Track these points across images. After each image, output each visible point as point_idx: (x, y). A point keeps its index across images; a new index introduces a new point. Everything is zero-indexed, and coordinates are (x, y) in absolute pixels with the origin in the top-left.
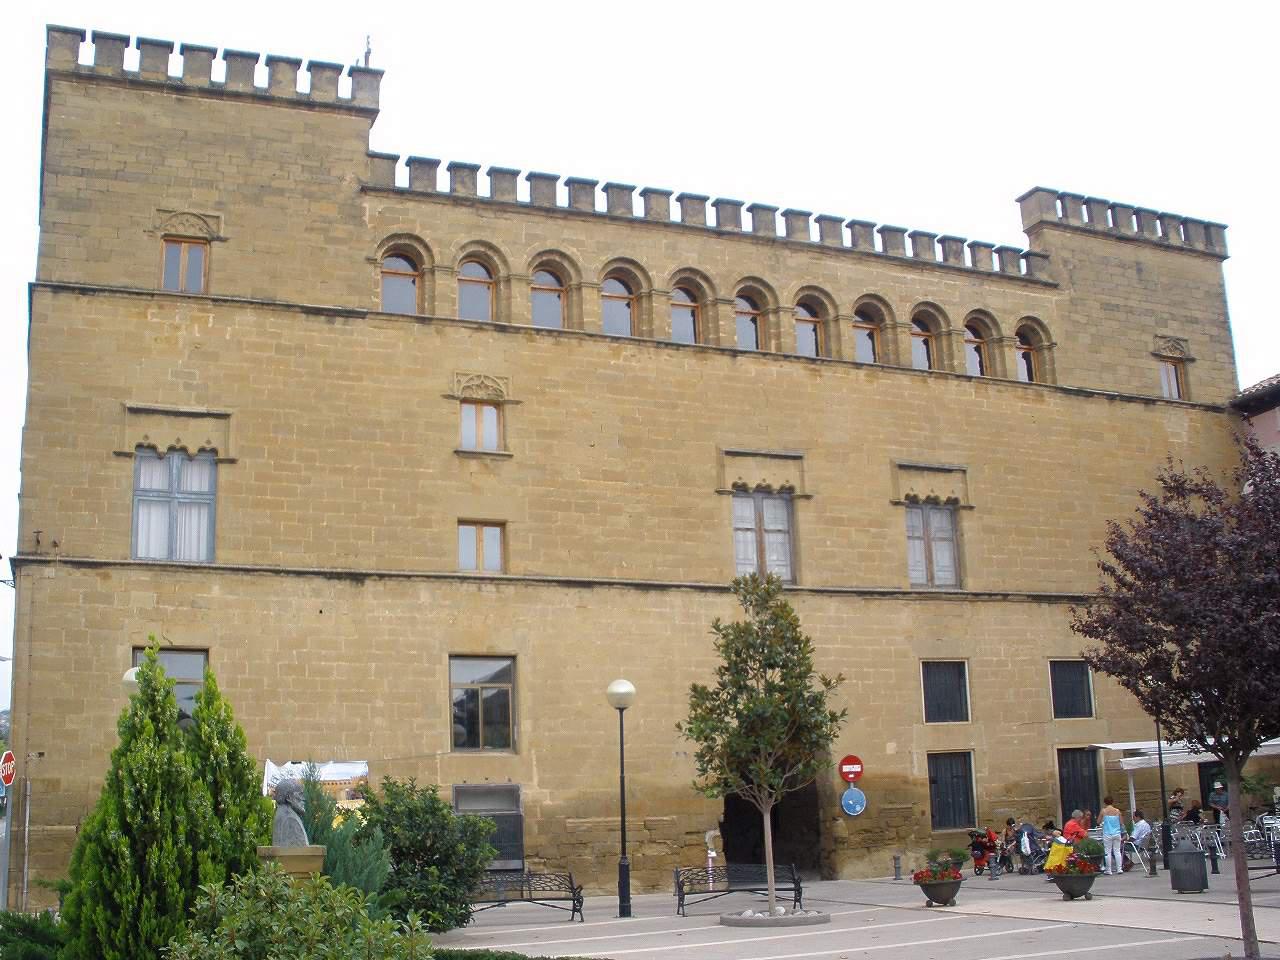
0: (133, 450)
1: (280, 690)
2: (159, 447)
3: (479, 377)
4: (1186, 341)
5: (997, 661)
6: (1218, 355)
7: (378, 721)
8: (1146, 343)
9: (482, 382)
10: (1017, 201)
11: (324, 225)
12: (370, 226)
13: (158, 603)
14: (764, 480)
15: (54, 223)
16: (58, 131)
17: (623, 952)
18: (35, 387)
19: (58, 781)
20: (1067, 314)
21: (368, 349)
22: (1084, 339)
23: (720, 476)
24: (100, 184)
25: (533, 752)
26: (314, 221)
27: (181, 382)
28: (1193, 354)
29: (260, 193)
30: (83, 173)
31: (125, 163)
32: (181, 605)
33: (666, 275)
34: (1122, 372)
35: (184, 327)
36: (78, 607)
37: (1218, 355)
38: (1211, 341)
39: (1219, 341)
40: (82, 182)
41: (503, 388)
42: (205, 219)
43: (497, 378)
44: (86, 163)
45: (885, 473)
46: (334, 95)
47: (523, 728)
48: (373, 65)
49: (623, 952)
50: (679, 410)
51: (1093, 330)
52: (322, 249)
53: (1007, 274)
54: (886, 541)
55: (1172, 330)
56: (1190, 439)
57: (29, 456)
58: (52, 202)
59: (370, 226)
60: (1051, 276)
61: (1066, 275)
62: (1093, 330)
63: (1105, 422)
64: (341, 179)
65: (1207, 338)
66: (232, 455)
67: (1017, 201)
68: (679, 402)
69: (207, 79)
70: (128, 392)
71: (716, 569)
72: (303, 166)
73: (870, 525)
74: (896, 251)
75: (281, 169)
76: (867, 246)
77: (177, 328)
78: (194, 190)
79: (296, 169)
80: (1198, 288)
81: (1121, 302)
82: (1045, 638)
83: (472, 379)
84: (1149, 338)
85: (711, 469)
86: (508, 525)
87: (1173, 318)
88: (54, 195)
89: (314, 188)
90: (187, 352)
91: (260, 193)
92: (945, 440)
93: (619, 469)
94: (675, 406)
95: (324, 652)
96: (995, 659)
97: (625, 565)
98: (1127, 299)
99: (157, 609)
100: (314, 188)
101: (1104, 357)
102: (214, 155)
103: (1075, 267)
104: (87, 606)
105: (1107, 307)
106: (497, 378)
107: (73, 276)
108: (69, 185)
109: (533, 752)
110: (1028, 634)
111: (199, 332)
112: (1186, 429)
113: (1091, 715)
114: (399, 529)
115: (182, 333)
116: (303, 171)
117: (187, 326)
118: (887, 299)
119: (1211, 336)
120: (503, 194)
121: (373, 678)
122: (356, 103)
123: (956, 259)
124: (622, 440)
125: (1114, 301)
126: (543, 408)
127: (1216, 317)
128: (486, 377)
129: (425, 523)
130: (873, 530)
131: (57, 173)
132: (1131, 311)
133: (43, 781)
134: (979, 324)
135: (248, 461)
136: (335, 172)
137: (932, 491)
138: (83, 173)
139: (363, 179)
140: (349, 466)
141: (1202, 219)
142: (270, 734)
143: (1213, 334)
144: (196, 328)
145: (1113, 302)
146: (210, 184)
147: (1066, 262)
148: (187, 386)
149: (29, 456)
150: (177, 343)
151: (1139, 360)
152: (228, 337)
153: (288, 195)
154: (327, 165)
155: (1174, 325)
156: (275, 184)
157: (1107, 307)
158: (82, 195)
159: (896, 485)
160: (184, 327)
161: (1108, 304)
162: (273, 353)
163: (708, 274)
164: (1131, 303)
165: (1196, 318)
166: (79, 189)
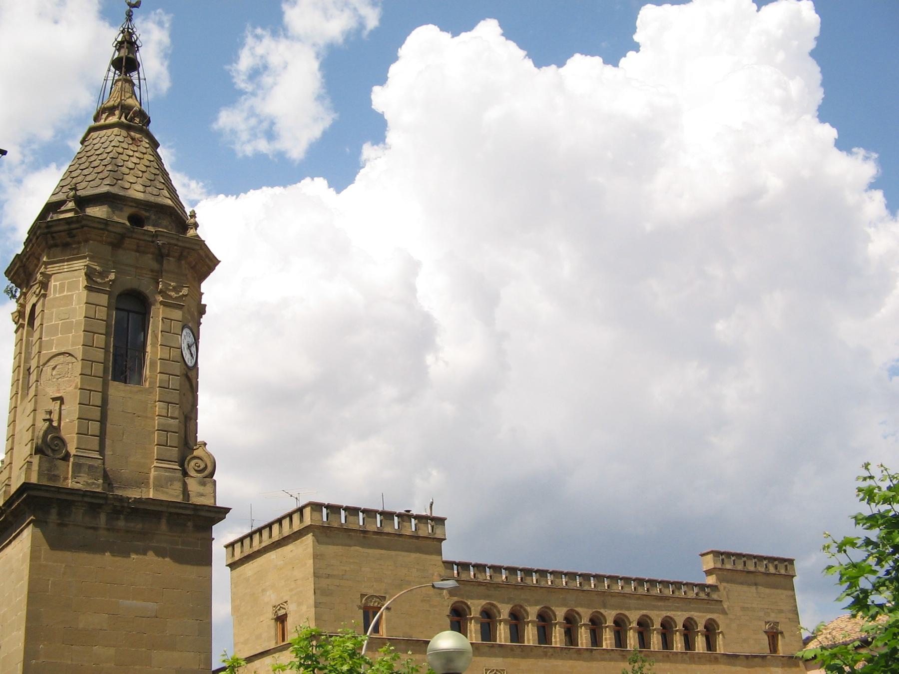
2: (156, 558)
12: (446, 598)
15: (320, 603)
17: (6, 542)
26: (424, 597)
30: (329, 576)
31: (346, 571)
42: (381, 598)
48: (436, 514)
49: (6, 542)
52: (429, 611)
53: (87, 214)
55: (773, 617)
59: (446, 598)
60: (719, 596)
65: (787, 620)
69: (375, 526)
72: (417, 569)
78: (375, 583)
81: (749, 606)
88: (319, 589)
97: (391, 648)
103: (729, 590)
105: (743, 609)
106: (501, 670)
108: (324, 583)
116: (417, 571)
119: (789, 618)
125: (746, 605)
138: (329, 576)
141: (751, 553)
143: (790, 617)
155: (773, 615)
157: (743, 609)
158: (330, 588)
161: (743, 608)
164: (754, 606)
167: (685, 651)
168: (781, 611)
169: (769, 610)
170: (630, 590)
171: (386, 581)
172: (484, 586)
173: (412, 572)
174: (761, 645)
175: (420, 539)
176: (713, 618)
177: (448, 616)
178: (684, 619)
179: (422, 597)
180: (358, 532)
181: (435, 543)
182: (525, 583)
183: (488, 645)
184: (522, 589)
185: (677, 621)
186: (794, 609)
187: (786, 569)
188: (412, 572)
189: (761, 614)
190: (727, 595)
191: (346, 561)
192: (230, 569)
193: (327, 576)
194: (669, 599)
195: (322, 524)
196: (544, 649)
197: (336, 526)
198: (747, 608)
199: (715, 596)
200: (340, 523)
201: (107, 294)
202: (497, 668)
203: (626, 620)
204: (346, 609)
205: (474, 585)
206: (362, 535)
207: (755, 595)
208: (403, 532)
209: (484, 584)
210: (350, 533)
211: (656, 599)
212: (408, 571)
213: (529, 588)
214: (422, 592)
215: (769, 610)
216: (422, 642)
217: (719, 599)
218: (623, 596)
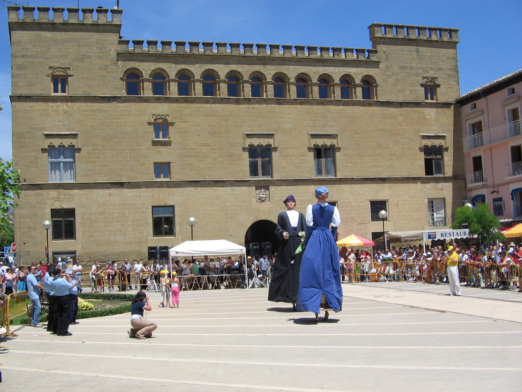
0: (47, 148)
1: (98, 220)
3: (159, 115)
4: (437, 78)
5: (448, 248)
6: (451, 82)
7: (130, 228)
8: (418, 80)
9: (161, 117)
10: (368, 28)
11: (104, 67)
12: (121, 66)
13: (58, 195)
14: (260, 143)
15: (16, 75)
16: (15, 43)
18: (15, 129)
19: (30, 252)
20: (384, 72)
21: (122, 109)
22: (391, 81)
23: (244, 142)
24: (30, 60)
25: (180, 236)
27: (61, 124)
28: (440, 83)
29: (83, 58)
30: (24, 56)
32: (65, 195)
33: (225, 74)
34: (407, 92)
35: (61, 106)
36: (33, 198)
37: (451, 82)
38: (449, 77)
39: (452, 77)
40: (24, 60)
41: (168, 118)
43: (166, 115)
44: (24, 53)
45: (306, 138)
46: (106, 20)
47: (176, 229)
50: (229, 121)
51: (395, 77)
54: (305, 162)
55: (431, 74)
56: (436, 116)
57: (14, 152)
58: (15, 67)
59: (121, 66)
60: (378, 58)
61: (384, 57)
62: (395, 77)
63: (398, 112)
64: (110, 50)
65: (446, 76)
66: (80, 147)
67: (368, 28)
68: (229, 118)
70: (44, 129)
71: (242, 174)
72: (97, 47)
73: (300, 156)
74: (313, 55)
75: (89, 49)
76: (302, 55)
77: (59, 106)
78: (61, 59)
79: (95, 48)
80: (444, 56)
81: (408, 65)
82: (368, 193)
83: (157, 116)
84: (420, 78)
85: (240, 140)
86: (171, 164)
87: (432, 69)
89: (101, 55)
90: (62, 114)
91: (83, 58)
92: (330, 124)
93: (208, 142)
94: (228, 120)
95: (111, 207)
96: (347, 201)
98: (411, 63)
99: (58, 197)
100: (101, 55)
101: (399, 87)
102: (66, 46)
104: (36, 198)
105: (402, 68)
106: (166, 115)
107: (24, 92)
109: (180, 236)
110: (362, 192)
111: (66, 107)
112: (434, 112)
113: (387, 220)
114: (134, 167)
115: (60, 108)
117: (62, 106)
118: (309, 74)
119: (449, 75)
120: (166, 51)
121: (127, 215)
122: (114, 23)
123: (338, 56)
124: (209, 133)
125: (405, 65)
126: (182, 124)
127: (451, 67)
128: (162, 115)
129: (143, 164)
130: (300, 158)
131: (15, 58)
132: (412, 68)
133: (25, 251)
134: (346, 80)
135: (84, 148)
136: (108, 48)
137: (324, 143)
138: (24, 56)
139: (118, 50)
140: (118, 148)
142: (95, 234)
144: (65, 106)
145: (404, 66)
146: (66, 57)
147: (384, 52)
148: (64, 125)
149: (14, 152)
150: (59, 111)
151: (415, 87)
152: (75, 108)
153: (92, 58)
154: (105, 46)
156: (88, 54)
157: (402, 68)
158: (24, 64)
159: (310, 141)
160: (61, 106)
162: (91, 113)
163: (240, 72)
164: (413, 65)
165: (443, 68)
166: (23, 62)
167: (340, 99)
168: (441, 69)
169: (428, 69)
170: (290, 54)
171: (70, 57)
172: (154, 56)
173: (92, 50)
174: (420, 94)
175: (100, 26)
176: (370, 74)
177: (122, 79)
178: (341, 75)
179: (100, 66)
180: (48, 24)
181: (113, 28)
182: (192, 53)
183: (157, 98)
184: (188, 57)
185: (334, 78)
186: (454, 67)
187: (451, 37)
188: (92, 50)
189: (420, 71)
190: (387, 58)
191: (38, 45)
192: (318, 200)
193: (23, 56)
194: (327, 61)
195: (18, 21)
196: (205, 99)
197: (29, 22)
198: (406, 67)
199: (374, 58)
200: (33, 19)
201: (311, 89)
202: (162, 114)
203: (285, 77)
204: (37, 78)
205: (146, 56)
206: (51, 26)
207: (415, 57)
208: (86, 22)
209: (154, 55)
210: (42, 26)
211: (315, 61)
212: (89, 49)
213: (195, 56)
214: (100, 63)
215: (428, 69)
216: (98, 97)
217: (377, 60)
218: (282, 60)
